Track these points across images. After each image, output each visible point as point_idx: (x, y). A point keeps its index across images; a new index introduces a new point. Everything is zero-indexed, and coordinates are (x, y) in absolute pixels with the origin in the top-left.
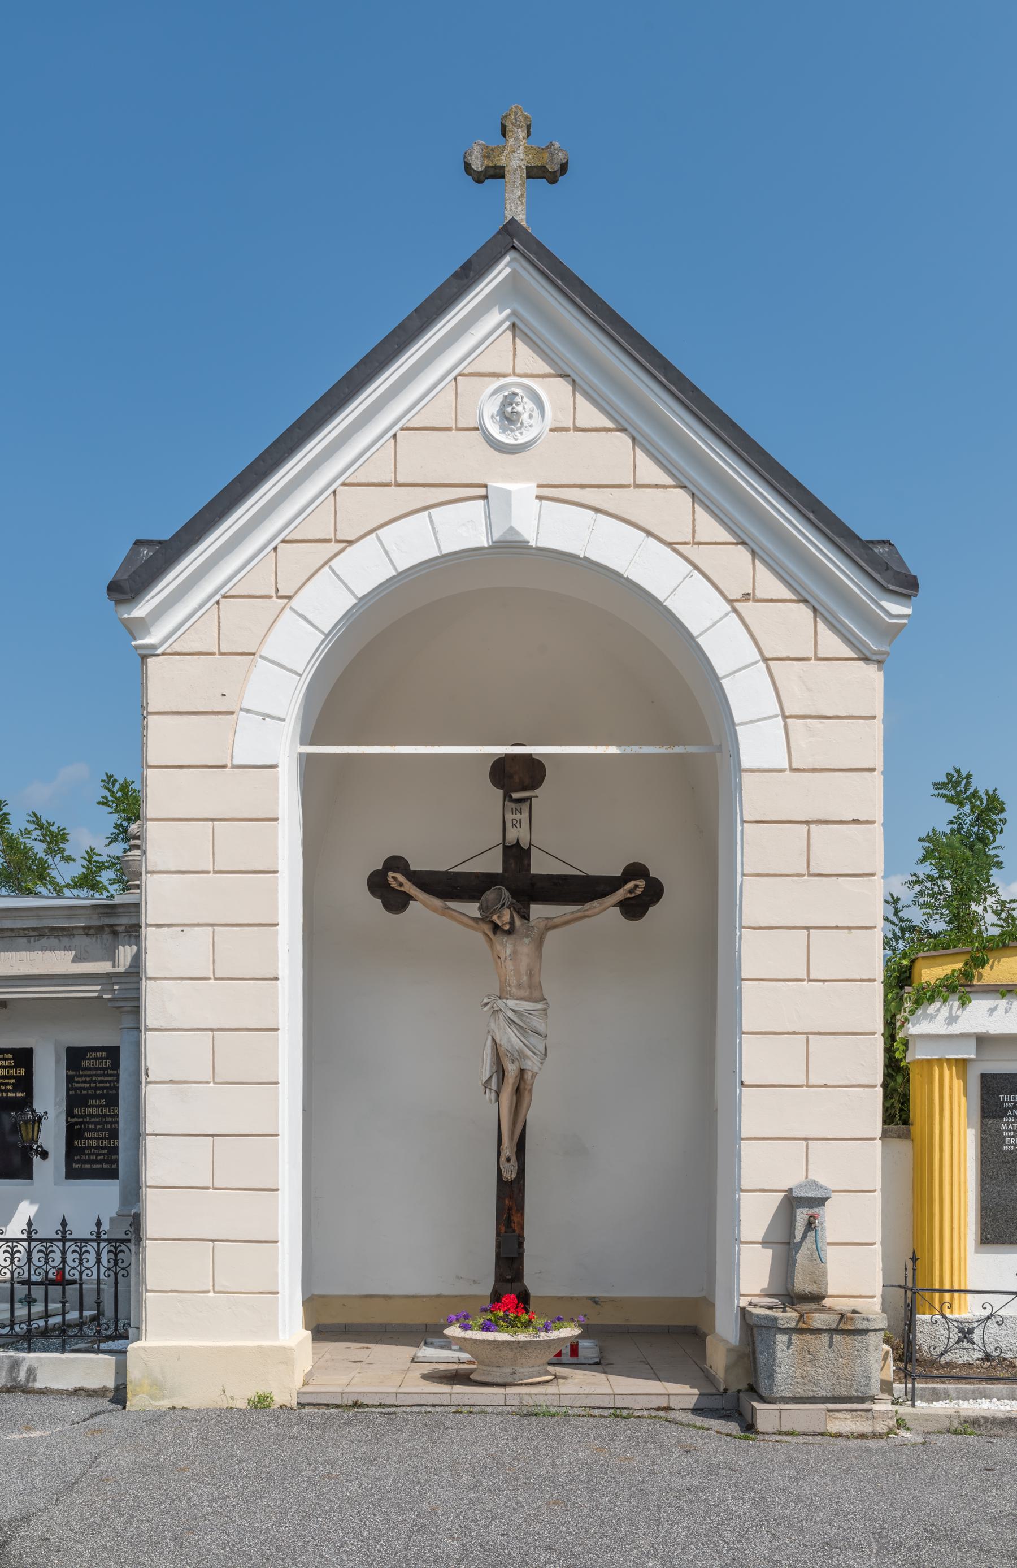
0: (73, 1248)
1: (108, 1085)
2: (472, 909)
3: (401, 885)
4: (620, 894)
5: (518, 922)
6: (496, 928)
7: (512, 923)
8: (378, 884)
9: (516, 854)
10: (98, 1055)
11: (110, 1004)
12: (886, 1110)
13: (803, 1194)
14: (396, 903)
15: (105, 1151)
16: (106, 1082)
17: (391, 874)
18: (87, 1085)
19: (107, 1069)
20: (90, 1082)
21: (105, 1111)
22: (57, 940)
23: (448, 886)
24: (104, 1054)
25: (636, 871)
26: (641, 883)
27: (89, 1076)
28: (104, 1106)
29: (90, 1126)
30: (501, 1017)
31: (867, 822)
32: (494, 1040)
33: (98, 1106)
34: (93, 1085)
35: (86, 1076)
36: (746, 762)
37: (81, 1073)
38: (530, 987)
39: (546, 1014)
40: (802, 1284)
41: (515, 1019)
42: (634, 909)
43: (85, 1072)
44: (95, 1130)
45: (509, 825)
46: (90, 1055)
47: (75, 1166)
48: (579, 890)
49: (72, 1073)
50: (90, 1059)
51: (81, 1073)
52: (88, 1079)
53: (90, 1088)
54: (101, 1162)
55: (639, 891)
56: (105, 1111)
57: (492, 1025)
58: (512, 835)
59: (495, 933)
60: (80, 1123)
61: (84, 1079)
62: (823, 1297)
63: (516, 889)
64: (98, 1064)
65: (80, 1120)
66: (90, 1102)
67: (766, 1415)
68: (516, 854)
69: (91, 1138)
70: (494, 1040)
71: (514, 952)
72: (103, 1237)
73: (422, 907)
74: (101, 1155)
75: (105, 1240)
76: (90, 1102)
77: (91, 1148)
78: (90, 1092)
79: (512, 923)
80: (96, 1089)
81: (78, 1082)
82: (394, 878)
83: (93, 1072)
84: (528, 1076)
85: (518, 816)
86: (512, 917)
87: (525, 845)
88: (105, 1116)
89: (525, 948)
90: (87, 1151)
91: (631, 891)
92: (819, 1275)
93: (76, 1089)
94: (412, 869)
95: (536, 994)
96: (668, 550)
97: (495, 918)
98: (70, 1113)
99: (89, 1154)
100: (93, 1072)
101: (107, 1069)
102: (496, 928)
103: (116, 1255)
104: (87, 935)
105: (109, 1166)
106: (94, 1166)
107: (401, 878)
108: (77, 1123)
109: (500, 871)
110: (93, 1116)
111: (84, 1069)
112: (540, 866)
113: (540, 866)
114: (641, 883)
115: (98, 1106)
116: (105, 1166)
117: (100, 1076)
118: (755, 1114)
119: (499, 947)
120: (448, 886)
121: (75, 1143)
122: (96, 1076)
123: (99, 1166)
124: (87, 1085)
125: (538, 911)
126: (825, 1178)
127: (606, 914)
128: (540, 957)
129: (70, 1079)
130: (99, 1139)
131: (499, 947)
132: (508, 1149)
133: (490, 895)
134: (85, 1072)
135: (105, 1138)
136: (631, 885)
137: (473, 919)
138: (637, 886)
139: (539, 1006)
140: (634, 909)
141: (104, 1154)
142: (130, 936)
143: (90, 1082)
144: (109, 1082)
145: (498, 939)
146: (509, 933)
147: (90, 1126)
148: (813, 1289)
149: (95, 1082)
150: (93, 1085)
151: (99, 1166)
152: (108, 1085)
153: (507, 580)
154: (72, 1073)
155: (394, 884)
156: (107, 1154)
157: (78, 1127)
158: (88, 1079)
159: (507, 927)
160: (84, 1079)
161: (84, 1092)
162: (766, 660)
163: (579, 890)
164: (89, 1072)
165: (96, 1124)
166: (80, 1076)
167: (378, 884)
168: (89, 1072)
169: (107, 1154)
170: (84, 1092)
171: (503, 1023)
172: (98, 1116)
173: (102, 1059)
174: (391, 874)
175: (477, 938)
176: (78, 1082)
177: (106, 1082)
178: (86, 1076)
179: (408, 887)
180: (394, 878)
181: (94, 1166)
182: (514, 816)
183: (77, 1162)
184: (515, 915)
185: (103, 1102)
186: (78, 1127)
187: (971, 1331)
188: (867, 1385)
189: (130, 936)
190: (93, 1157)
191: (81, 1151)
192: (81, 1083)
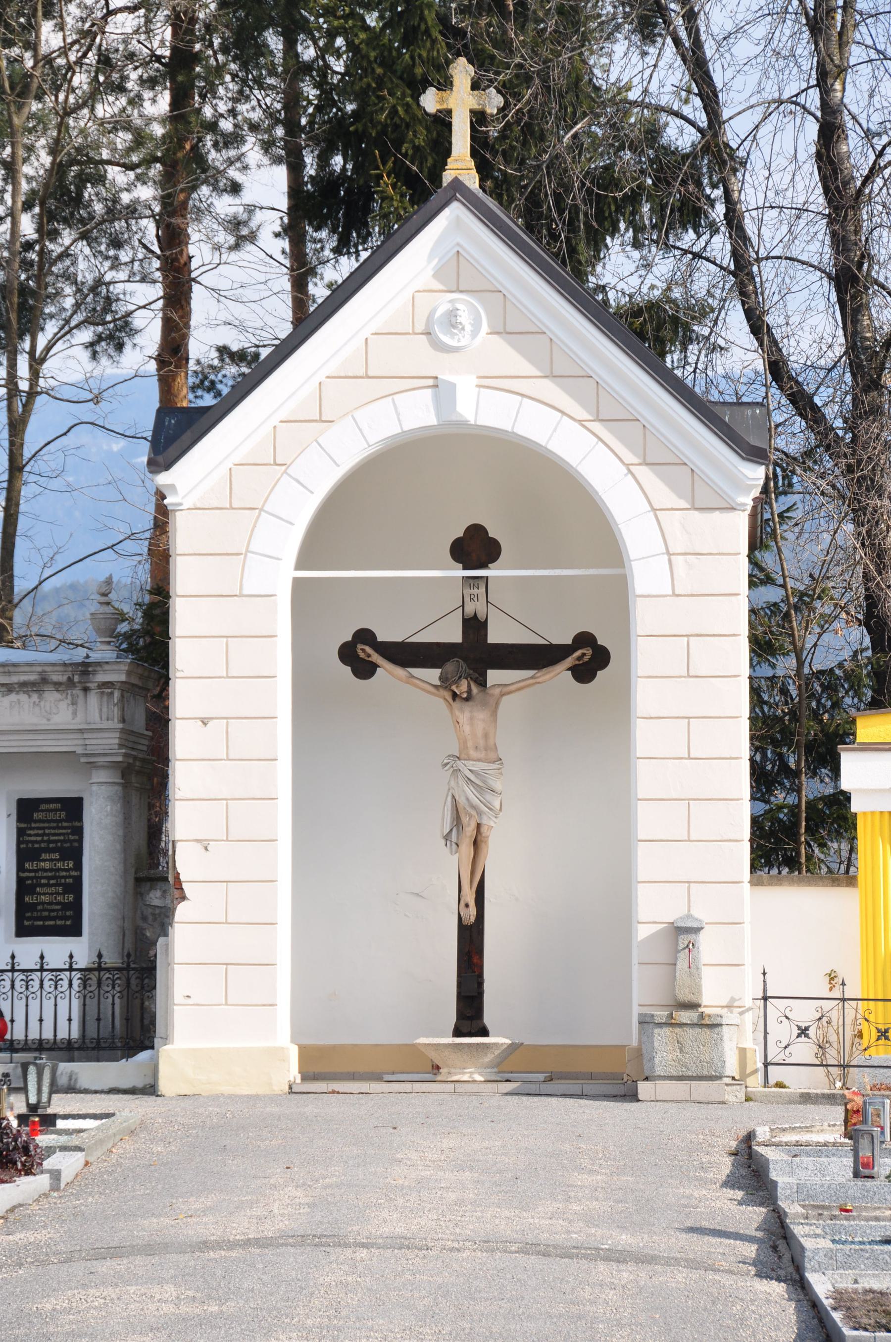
0: (107, 975)
1: (62, 838)
2: (433, 675)
3: (369, 656)
4: (570, 661)
5: (475, 689)
6: (455, 696)
7: (469, 691)
8: (347, 653)
9: (474, 626)
10: (52, 806)
11: (83, 760)
12: (23, 888)
13: (683, 925)
14: (364, 670)
15: (59, 907)
16: (60, 835)
17: (360, 646)
18: (39, 838)
19: (61, 821)
20: (42, 835)
21: (59, 865)
22: (26, 696)
23: (408, 655)
24: (59, 806)
25: (585, 639)
26: (588, 652)
27: (43, 828)
28: (58, 860)
29: (43, 881)
30: (460, 778)
31: (734, 635)
32: (453, 796)
33: (51, 860)
34: (46, 838)
35: (38, 828)
36: (639, 590)
37: (33, 825)
38: (486, 750)
39: (501, 774)
40: (684, 996)
41: (472, 777)
42: (584, 673)
43: (37, 825)
44: (48, 885)
45: (467, 599)
46: (43, 807)
47: (26, 923)
48: (536, 657)
49: (23, 825)
50: (43, 811)
51: (33, 825)
52: (40, 832)
53: (43, 841)
54: (54, 919)
55: (586, 659)
56: (59, 865)
57: (452, 783)
58: (470, 609)
59: (454, 700)
60: (31, 878)
61: (36, 832)
62: (700, 1006)
63: (472, 659)
64: (51, 816)
65: (33, 874)
66: (43, 856)
67: (644, 1089)
68: (474, 626)
69: (44, 894)
70: (453, 796)
71: (471, 719)
72: (132, 966)
73: (387, 673)
74: (54, 911)
75: (133, 969)
76: (43, 856)
77: (43, 903)
78: (43, 845)
79: (469, 691)
80: (49, 842)
81: (30, 835)
82: (363, 650)
83: (46, 825)
84: (484, 829)
85: (475, 591)
86: (469, 686)
87: (481, 616)
88: (59, 870)
89: (481, 715)
90: (39, 908)
91: (579, 659)
92: (697, 989)
93: (27, 842)
94: (379, 639)
95: (492, 756)
96: (577, 425)
97: (454, 688)
98: (20, 868)
99: (41, 911)
100: (46, 825)
101: (61, 821)
102: (455, 696)
103: (143, 980)
104: (57, 690)
105: (62, 922)
106: (47, 923)
107: (369, 650)
108: (28, 878)
109: (460, 641)
110: (45, 870)
111: (36, 821)
112: (496, 635)
113: (496, 635)
114: (588, 652)
115: (51, 860)
116: (59, 923)
117: (54, 828)
118: (647, 862)
119: (457, 713)
120: (408, 655)
121: (27, 899)
122: (49, 828)
123: (52, 923)
124: (39, 838)
125: (494, 676)
126: (700, 913)
127: (560, 676)
128: (495, 721)
129: (20, 833)
130: (52, 894)
131: (457, 713)
132: (470, 896)
133: (450, 667)
134: (37, 825)
135: (58, 894)
136: (578, 653)
137: (436, 687)
138: (584, 654)
139: (496, 766)
140: (584, 673)
141: (57, 910)
142: (102, 693)
143: (42, 835)
144: (63, 834)
145: (457, 705)
146: (467, 699)
147: (43, 881)
148: (693, 998)
149: (48, 835)
150: (46, 838)
151: (52, 923)
152: (62, 838)
153: (447, 447)
154: (23, 825)
155: (362, 655)
156: (61, 910)
157: (29, 882)
158: (40, 832)
159: (465, 695)
160: (36, 832)
161: (36, 846)
162: (654, 510)
163: (536, 657)
164: (42, 825)
165: (49, 878)
166: (32, 829)
167: (347, 653)
168: (42, 825)
169: (61, 910)
170: (36, 846)
171: (462, 782)
172: (51, 870)
173: (56, 810)
174: (360, 646)
175: (439, 703)
176: (30, 835)
177: (60, 835)
178: (38, 828)
179: (376, 658)
180: (363, 650)
181: (47, 923)
182: (472, 591)
183: (29, 919)
184: (472, 684)
185: (57, 856)
186: (29, 882)
187: (807, 1029)
188: (723, 1067)
189: (102, 693)
190: (46, 914)
191: (33, 907)
192: (33, 835)
